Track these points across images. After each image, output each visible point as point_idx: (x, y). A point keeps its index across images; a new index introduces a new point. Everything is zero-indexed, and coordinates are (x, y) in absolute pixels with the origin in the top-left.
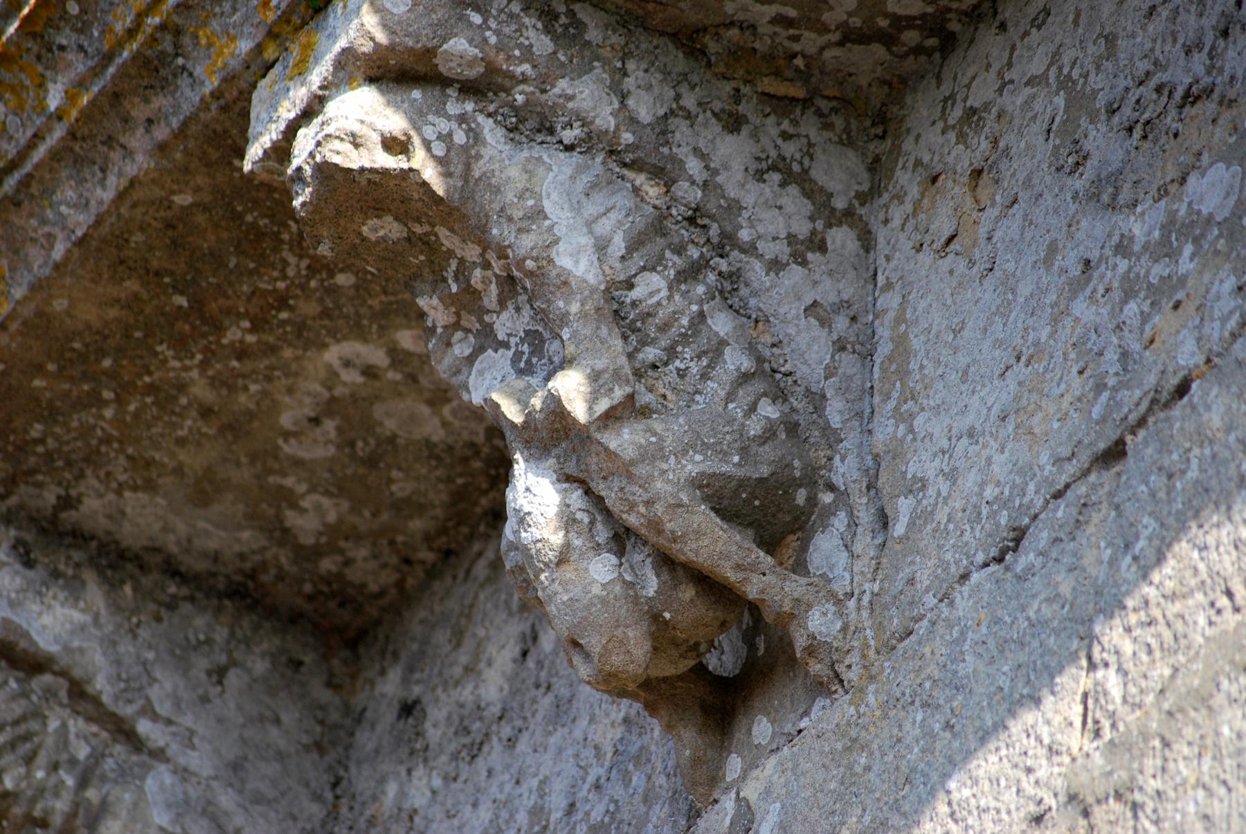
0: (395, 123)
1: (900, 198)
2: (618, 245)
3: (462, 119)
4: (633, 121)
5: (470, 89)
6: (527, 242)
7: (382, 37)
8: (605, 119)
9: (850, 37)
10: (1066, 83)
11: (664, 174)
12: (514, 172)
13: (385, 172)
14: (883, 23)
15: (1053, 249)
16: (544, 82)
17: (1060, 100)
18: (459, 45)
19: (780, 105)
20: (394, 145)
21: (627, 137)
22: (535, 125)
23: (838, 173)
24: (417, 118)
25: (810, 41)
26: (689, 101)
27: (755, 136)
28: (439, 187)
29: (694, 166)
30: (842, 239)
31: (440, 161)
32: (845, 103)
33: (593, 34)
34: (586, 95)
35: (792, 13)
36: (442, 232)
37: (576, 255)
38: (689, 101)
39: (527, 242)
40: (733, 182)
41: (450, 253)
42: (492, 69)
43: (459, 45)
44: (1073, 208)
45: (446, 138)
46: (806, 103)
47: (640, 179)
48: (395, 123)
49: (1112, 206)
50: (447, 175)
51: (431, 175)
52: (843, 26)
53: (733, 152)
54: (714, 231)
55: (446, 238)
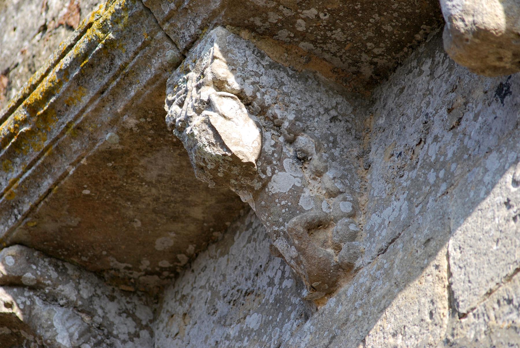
0: (8, 298)
1: (162, 321)
2: (76, 336)
3: (29, 297)
4: (81, 298)
5: (32, 288)
6: (48, 335)
7: (5, 273)
8: (73, 297)
9: (148, 273)
10: (211, 288)
11: (91, 314)
12: (45, 313)
13: (5, 314)
14: (157, 269)
15: (207, 338)
16: (55, 286)
17: (209, 293)
18: (29, 275)
19: (127, 293)
20: (8, 305)
21: (80, 303)
22: (51, 299)
23: (144, 314)
24: (15, 297)
25: (136, 274)
26: (99, 292)
27: (119, 302)
28: (21, 318)
29: (100, 312)
30: (144, 333)
31: (23, 311)
32: (146, 293)
33: (70, 272)
34: (67, 290)
35: (130, 266)
36: (22, 332)
37: (63, 339)
38: (99, 292)
39: (48, 335)
40: (112, 317)
41: (24, 338)
42: (39, 282)
43: (29, 275)
44: (213, 325)
45: (24, 303)
46: (134, 293)
47: (83, 315)
48: (8, 298)
49: (224, 325)
50: (24, 314)
51: (19, 314)
52: (146, 270)
53: (112, 307)
54: (106, 331)
55: (23, 334)
